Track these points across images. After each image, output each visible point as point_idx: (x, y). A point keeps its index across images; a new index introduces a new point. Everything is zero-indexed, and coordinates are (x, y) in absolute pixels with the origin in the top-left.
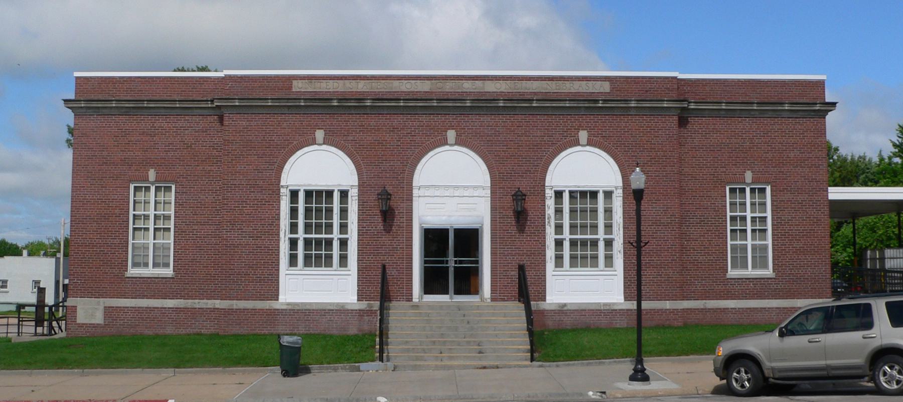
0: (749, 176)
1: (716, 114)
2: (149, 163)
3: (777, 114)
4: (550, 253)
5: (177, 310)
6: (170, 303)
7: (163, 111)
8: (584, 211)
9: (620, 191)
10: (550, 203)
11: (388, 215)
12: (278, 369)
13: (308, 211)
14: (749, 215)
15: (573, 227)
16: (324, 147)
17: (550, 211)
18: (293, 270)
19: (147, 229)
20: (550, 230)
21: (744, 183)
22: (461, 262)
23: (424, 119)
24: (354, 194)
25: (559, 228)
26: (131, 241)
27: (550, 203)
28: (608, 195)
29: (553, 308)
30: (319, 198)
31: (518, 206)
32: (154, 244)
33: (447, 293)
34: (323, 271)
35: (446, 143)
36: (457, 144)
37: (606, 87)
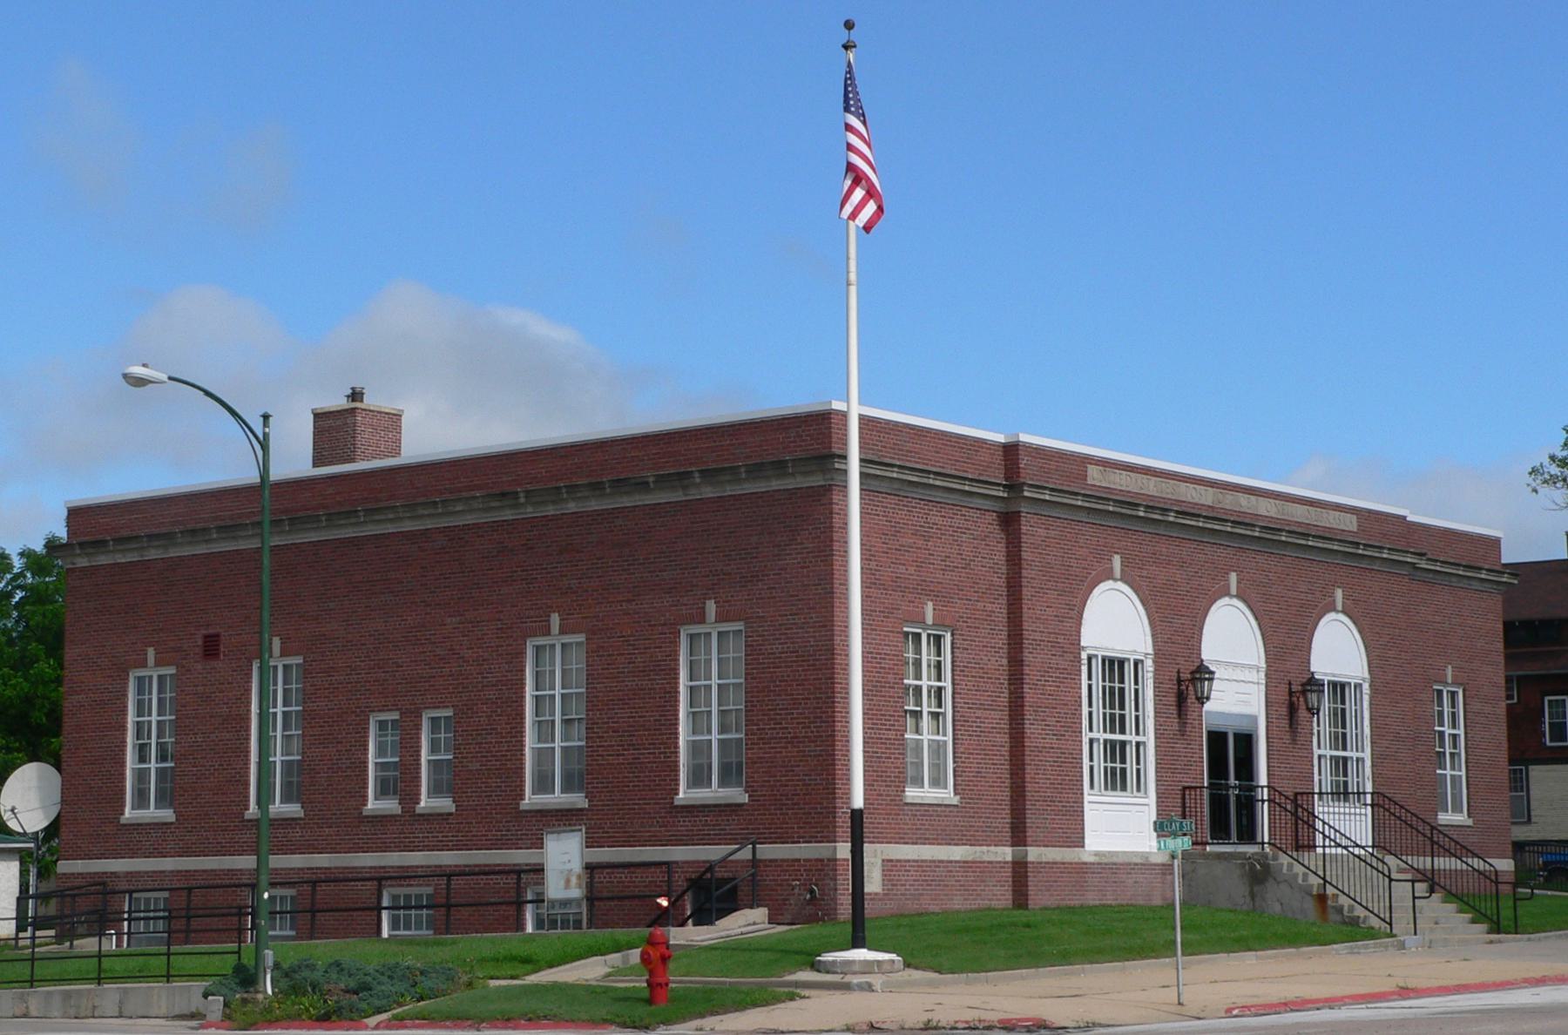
7: (939, 496)
10: (1092, 709)
27: (1092, 709)
28: (1358, 686)
29: (1092, 859)
30: (1114, 666)
37: (1350, 523)
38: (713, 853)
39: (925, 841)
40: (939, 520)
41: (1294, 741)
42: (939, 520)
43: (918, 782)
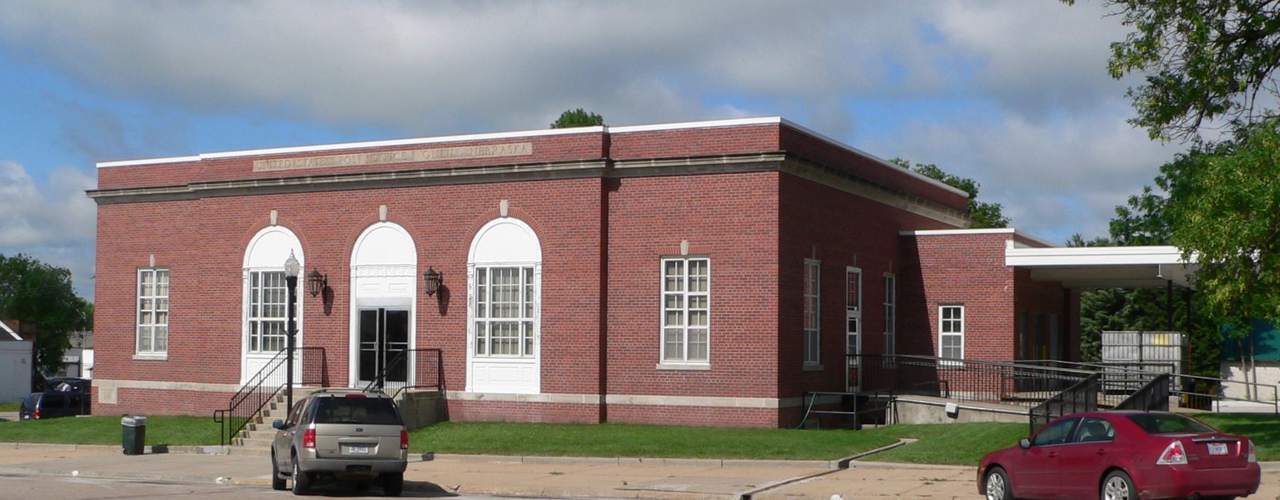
0: (684, 247)
2: (149, 249)
3: (719, 170)
4: (471, 338)
5: (170, 391)
6: (164, 385)
9: (539, 268)
11: (328, 295)
12: (120, 448)
13: (495, 290)
14: (686, 294)
15: (495, 309)
16: (278, 228)
17: (472, 292)
18: (482, 358)
19: (681, 313)
20: (471, 311)
21: (680, 255)
22: (395, 347)
23: (360, 194)
24: (538, 271)
25: (481, 309)
26: (139, 325)
31: (439, 288)
32: (689, 331)
34: (508, 357)
36: (388, 220)
37: (528, 149)
41: (443, 311)
43: (144, 347)
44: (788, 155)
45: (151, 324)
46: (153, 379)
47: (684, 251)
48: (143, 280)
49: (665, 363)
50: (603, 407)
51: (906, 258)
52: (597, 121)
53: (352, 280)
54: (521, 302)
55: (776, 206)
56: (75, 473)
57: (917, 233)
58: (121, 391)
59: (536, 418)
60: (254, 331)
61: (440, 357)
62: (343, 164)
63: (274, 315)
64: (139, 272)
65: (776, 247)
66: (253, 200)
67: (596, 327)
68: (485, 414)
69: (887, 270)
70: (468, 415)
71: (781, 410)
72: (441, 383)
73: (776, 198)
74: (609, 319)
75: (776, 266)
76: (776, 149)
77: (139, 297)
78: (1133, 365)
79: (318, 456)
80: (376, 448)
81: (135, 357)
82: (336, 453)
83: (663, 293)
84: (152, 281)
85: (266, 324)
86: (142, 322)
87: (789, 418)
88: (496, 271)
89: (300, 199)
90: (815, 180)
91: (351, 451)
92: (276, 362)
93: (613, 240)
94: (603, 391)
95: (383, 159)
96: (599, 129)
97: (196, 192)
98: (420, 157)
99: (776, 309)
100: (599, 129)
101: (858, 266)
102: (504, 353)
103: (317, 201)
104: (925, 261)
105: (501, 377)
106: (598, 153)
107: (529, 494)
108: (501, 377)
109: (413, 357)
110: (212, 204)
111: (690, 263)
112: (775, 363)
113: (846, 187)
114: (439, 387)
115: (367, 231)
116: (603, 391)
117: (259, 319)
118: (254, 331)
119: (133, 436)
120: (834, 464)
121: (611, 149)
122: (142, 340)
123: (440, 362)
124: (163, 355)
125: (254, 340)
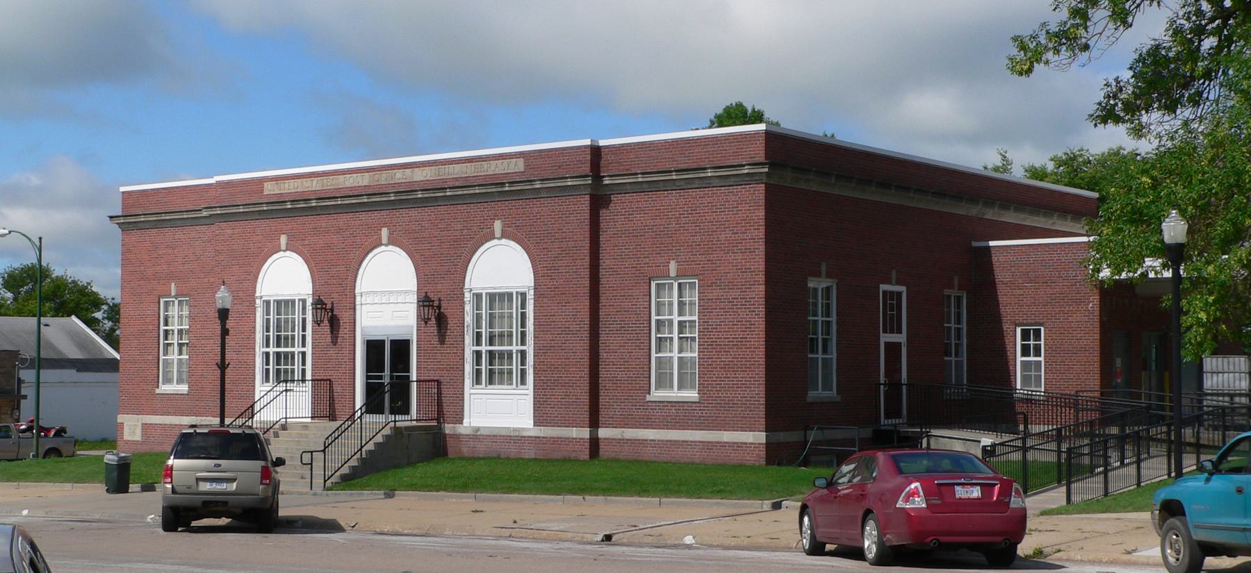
0: (673, 266)
1: (638, 188)
2: (170, 277)
3: (705, 183)
4: (468, 368)
7: (179, 223)
8: (502, 316)
9: (532, 292)
11: (334, 323)
17: (469, 319)
18: (479, 390)
19: (671, 339)
20: (468, 339)
21: (668, 277)
23: (363, 216)
26: (162, 357)
28: (523, 295)
29: (467, 432)
31: (437, 312)
32: (680, 358)
33: (383, 413)
35: (494, 238)
37: (520, 165)
38: (187, 420)
39: (169, 414)
40: (182, 236)
41: (442, 342)
42: (182, 236)
43: (168, 381)
44: (772, 165)
45: (174, 356)
46: (175, 414)
47: (673, 273)
48: (166, 311)
49: (657, 394)
50: (594, 443)
51: (979, 276)
52: (758, 117)
53: (358, 307)
54: (297, 333)
55: (762, 222)
56: (25, 512)
57: (992, 243)
58: (145, 427)
59: (529, 453)
60: (478, 362)
61: (439, 388)
62: (348, 184)
63: (286, 346)
64: (162, 301)
65: (762, 267)
66: (263, 225)
67: (589, 358)
68: (481, 449)
69: (951, 287)
70: (465, 451)
71: (769, 445)
72: (440, 417)
73: (762, 213)
74: (602, 347)
75: (762, 288)
76: (762, 159)
77: (162, 328)
78: (1241, 395)
79: (174, 491)
80: (235, 485)
81: (158, 391)
82: (193, 490)
83: (654, 318)
84: (174, 311)
85: (278, 354)
86: (166, 353)
87: (776, 454)
88: (492, 297)
89: (309, 222)
90: (823, 189)
91: (206, 487)
92: (272, 395)
93: (606, 261)
94: (594, 423)
95: (384, 178)
96: (761, 127)
97: (211, 216)
98: (420, 175)
99: (763, 335)
100: (761, 127)
101: (899, 283)
102: (501, 383)
103: (324, 225)
104: (1001, 275)
105: (498, 410)
106: (586, 169)
107: (415, 532)
108: (498, 410)
109: (414, 386)
110: (227, 229)
111: (680, 284)
112: (763, 394)
113: (892, 198)
114: (438, 420)
115: (370, 255)
116: (594, 423)
117: (484, 348)
118: (478, 362)
119: (115, 474)
120: (767, 504)
121: (602, 163)
122: (659, 376)
123: (439, 394)
124: (184, 388)
125: (478, 372)
